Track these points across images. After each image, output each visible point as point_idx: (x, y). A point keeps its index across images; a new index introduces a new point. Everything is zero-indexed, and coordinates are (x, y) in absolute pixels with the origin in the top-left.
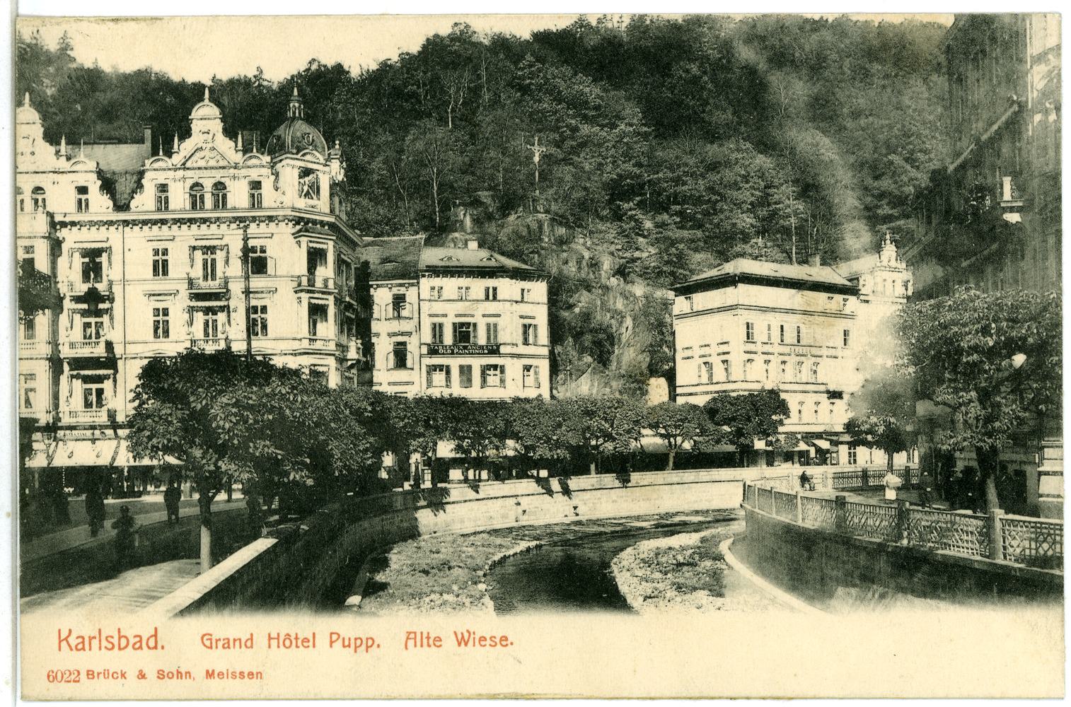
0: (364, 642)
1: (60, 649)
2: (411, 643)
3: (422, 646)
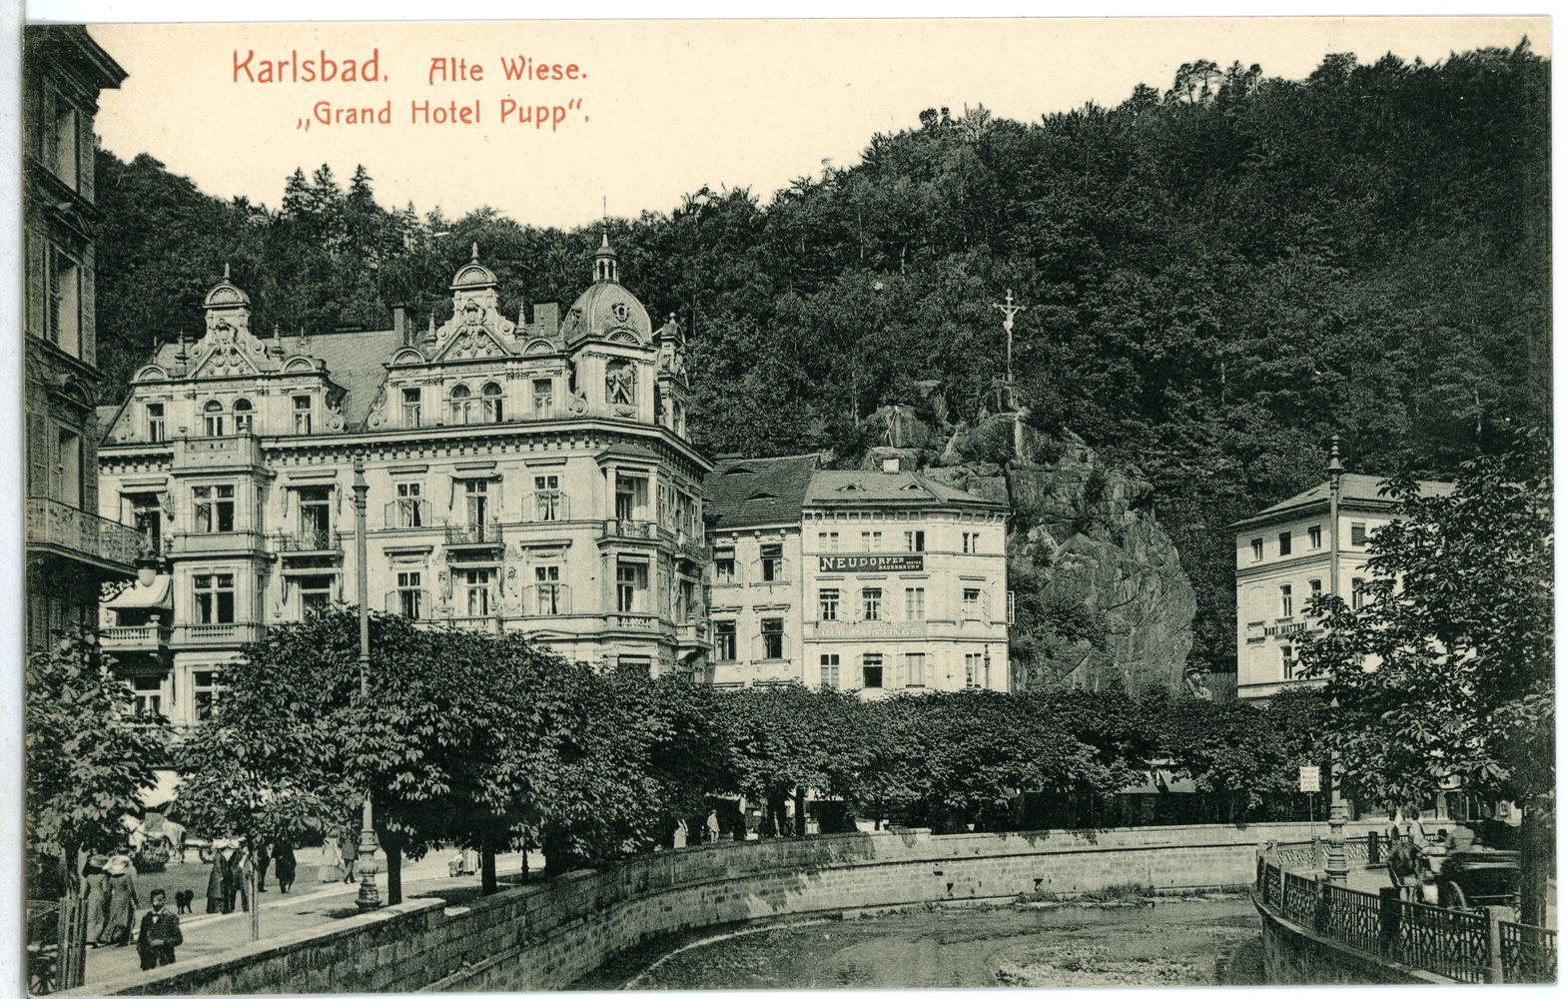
1: (235, 79)
2: (438, 74)
3: (454, 79)
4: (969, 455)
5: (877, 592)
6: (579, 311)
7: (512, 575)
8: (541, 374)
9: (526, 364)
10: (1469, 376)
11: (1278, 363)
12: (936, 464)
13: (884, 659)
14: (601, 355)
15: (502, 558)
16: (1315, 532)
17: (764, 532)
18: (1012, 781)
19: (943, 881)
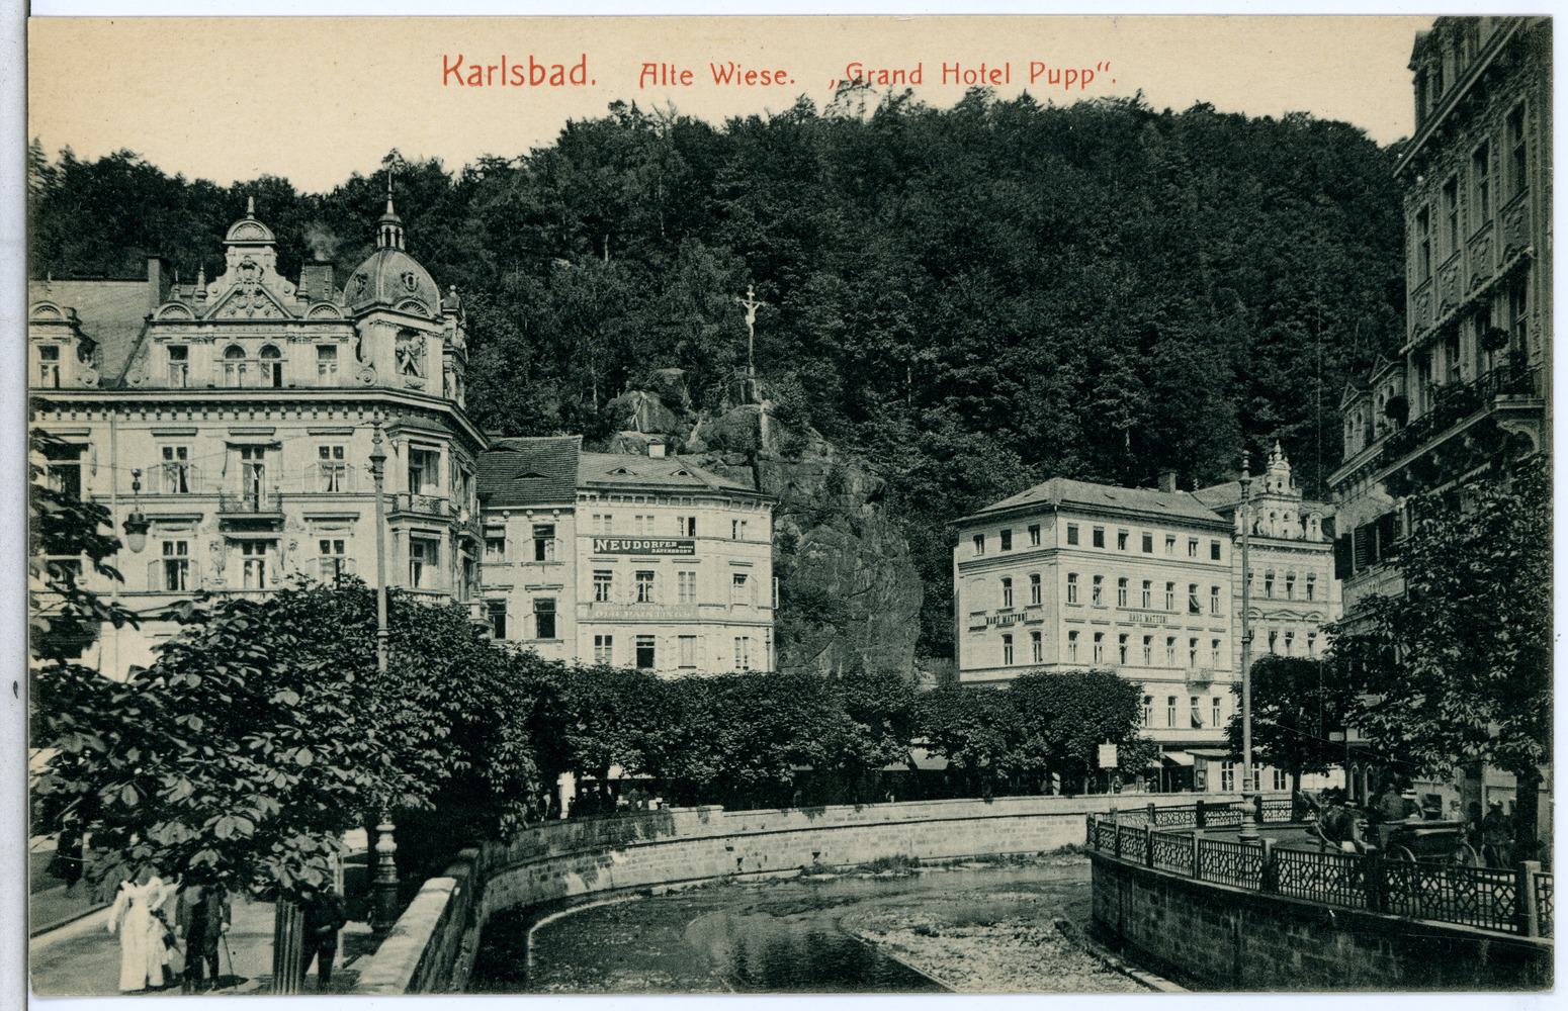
0: (567, 79)
1: (445, 82)
2: (648, 78)
3: (664, 82)
4: (716, 443)
5: (650, 575)
6: (365, 277)
7: (293, 547)
8: (326, 340)
9: (307, 328)
10: (1125, 393)
11: (964, 371)
12: (682, 451)
13: (656, 640)
14: (390, 325)
15: (282, 529)
16: (1034, 530)
17: (535, 511)
18: (796, 757)
19: (734, 856)
